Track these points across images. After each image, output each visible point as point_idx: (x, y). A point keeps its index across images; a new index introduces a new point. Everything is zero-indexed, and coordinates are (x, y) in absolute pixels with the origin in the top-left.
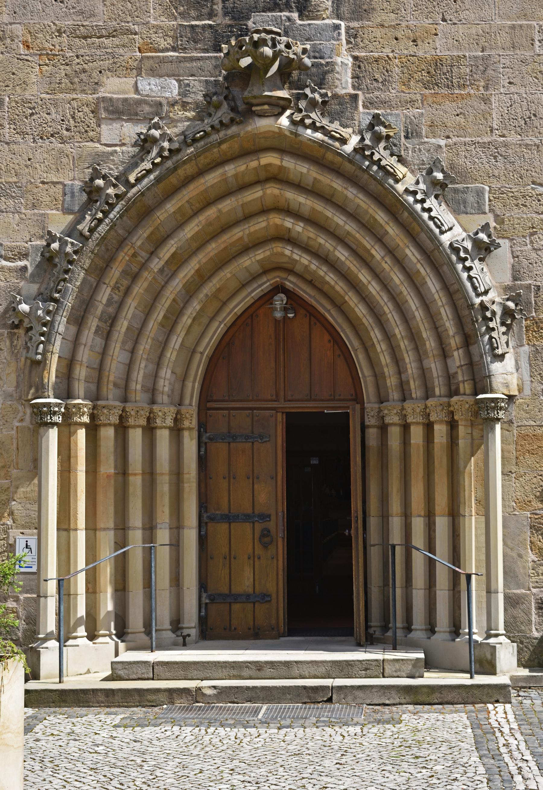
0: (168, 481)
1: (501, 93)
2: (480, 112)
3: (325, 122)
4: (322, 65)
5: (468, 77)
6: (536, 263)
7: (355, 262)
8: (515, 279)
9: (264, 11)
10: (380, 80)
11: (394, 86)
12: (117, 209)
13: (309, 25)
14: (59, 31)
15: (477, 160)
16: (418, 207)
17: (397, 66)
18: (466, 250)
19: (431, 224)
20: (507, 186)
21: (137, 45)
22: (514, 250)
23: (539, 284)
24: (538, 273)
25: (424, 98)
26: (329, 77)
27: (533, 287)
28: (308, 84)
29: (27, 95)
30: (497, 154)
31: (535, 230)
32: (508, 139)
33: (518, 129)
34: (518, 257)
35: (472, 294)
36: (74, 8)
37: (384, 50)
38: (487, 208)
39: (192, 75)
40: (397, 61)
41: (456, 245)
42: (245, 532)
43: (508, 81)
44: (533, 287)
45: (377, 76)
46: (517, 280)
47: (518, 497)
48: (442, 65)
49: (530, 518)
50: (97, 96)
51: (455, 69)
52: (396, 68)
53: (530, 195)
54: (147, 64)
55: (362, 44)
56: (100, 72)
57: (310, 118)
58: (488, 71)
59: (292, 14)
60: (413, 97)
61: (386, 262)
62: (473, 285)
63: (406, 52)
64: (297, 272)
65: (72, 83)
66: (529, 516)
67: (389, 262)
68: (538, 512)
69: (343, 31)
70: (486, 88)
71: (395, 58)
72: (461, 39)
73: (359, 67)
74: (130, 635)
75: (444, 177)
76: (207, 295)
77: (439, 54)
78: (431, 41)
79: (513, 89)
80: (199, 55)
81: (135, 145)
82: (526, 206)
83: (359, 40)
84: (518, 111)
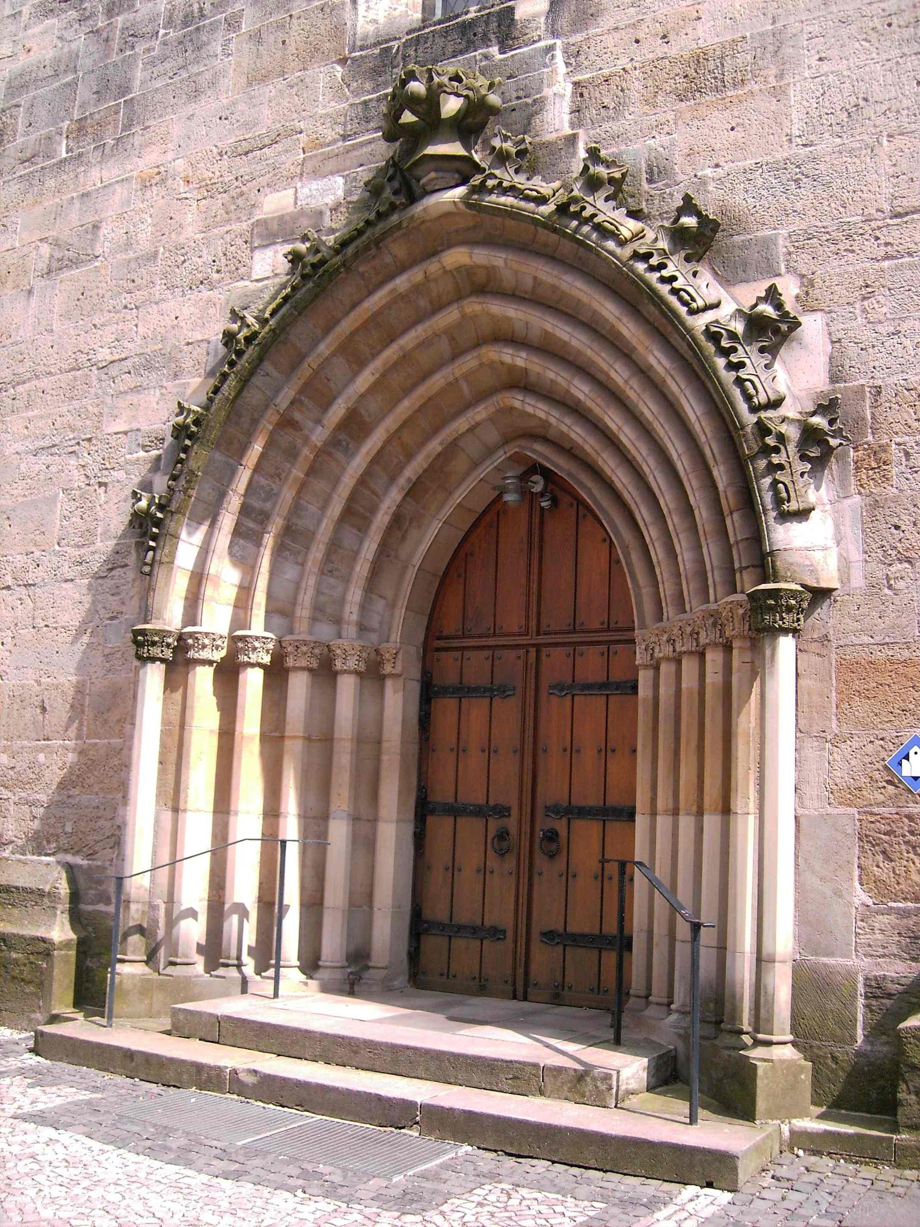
0: (349, 751)
1: (806, 78)
2: (771, 115)
3: (520, 180)
4: (527, 104)
5: (749, 68)
6: (874, 346)
7: (599, 401)
8: (834, 378)
9: (454, 57)
10: (612, 105)
11: (632, 109)
12: (246, 357)
13: (513, 56)
14: (220, 154)
15: (764, 193)
16: (653, 277)
17: (637, 79)
18: (733, 336)
19: (673, 300)
20: (820, 224)
21: (302, 145)
22: (833, 329)
23: (879, 382)
24: (877, 364)
25: (678, 115)
26: (536, 121)
27: (867, 389)
28: (496, 131)
29: (182, 239)
30: (799, 176)
31: (869, 290)
32: (818, 147)
33: (837, 129)
34: (839, 341)
35: (742, 407)
36: (238, 121)
37: (619, 62)
38: (783, 269)
39: (361, 165)
40: (637, 72)
41: (713, 329)
42: (471, 831)
43: (817, 57)
44: (867, 389)
45: (606, 101)
46: (838, 382)
47: (838, 781)
48: (707, 60)
49: (860, 820)
50: (252, 221)
51: (728, 62)
52: (636, 83)
53: (861, 231)
54: (309, 166)
55: (586, 63)
56: (259, 191)
57: (496, 177)
58: (782, 51)
59: (490, 49)
60: (662, 118)
61: (631, 388)
62: (744, 392)
63: (651, 56)
64: (552, 438)
65: (227, 213)
66: (857, 816)
67: (635, 387)
68: (875, 810)
69: (558, 53)
70: (780, 76)
71: (635, 68)
72: (737, 15)
73: (581, 95)
74: (371, 971)
75: (699, 223)
76: (409, 480)
77: (702, 46)
78: (690, 31)
79: (825, 67)
80: (371, 137)
81: (287, 274)
82: (853, 251)
83: (582, 58)
84: (835, 100)
